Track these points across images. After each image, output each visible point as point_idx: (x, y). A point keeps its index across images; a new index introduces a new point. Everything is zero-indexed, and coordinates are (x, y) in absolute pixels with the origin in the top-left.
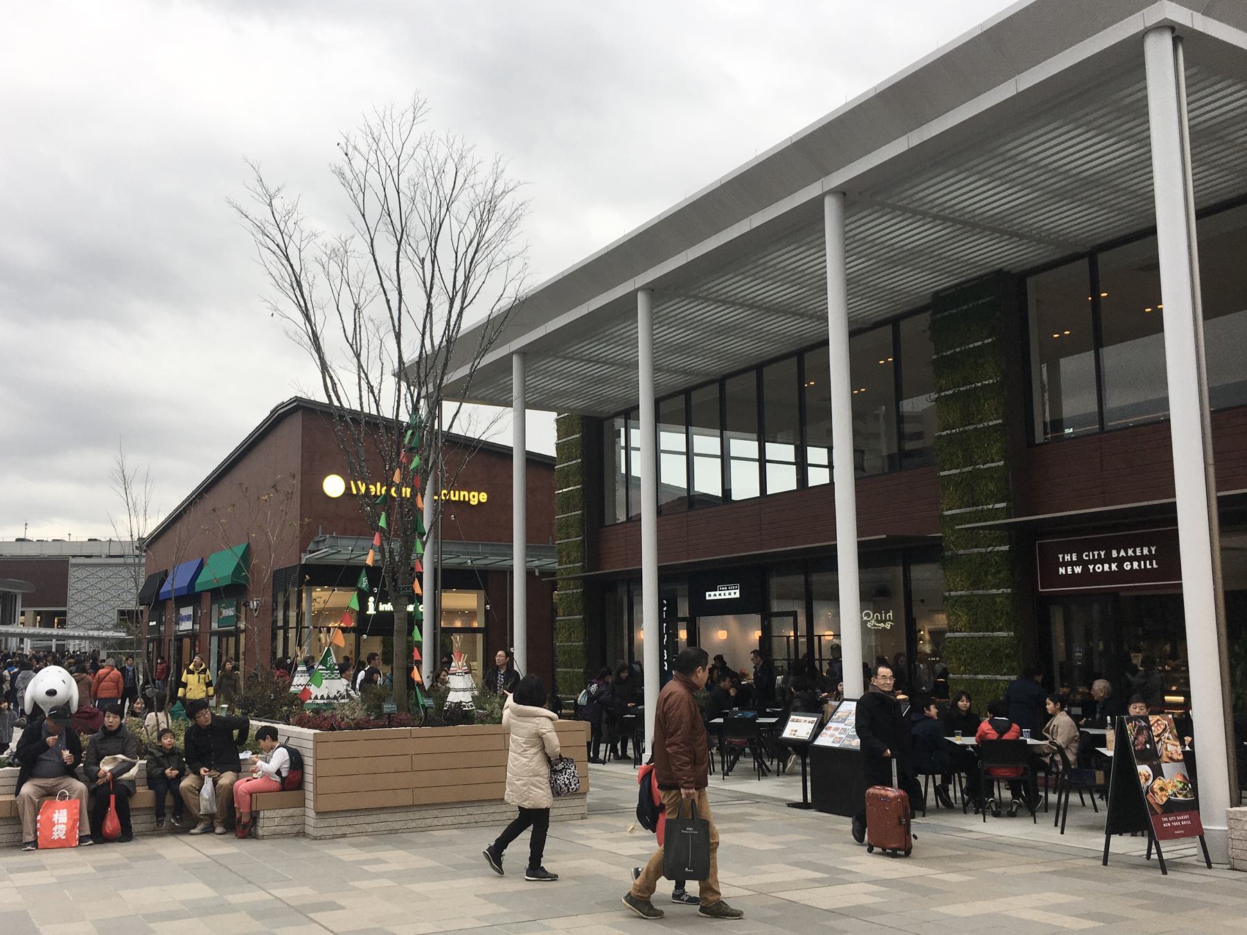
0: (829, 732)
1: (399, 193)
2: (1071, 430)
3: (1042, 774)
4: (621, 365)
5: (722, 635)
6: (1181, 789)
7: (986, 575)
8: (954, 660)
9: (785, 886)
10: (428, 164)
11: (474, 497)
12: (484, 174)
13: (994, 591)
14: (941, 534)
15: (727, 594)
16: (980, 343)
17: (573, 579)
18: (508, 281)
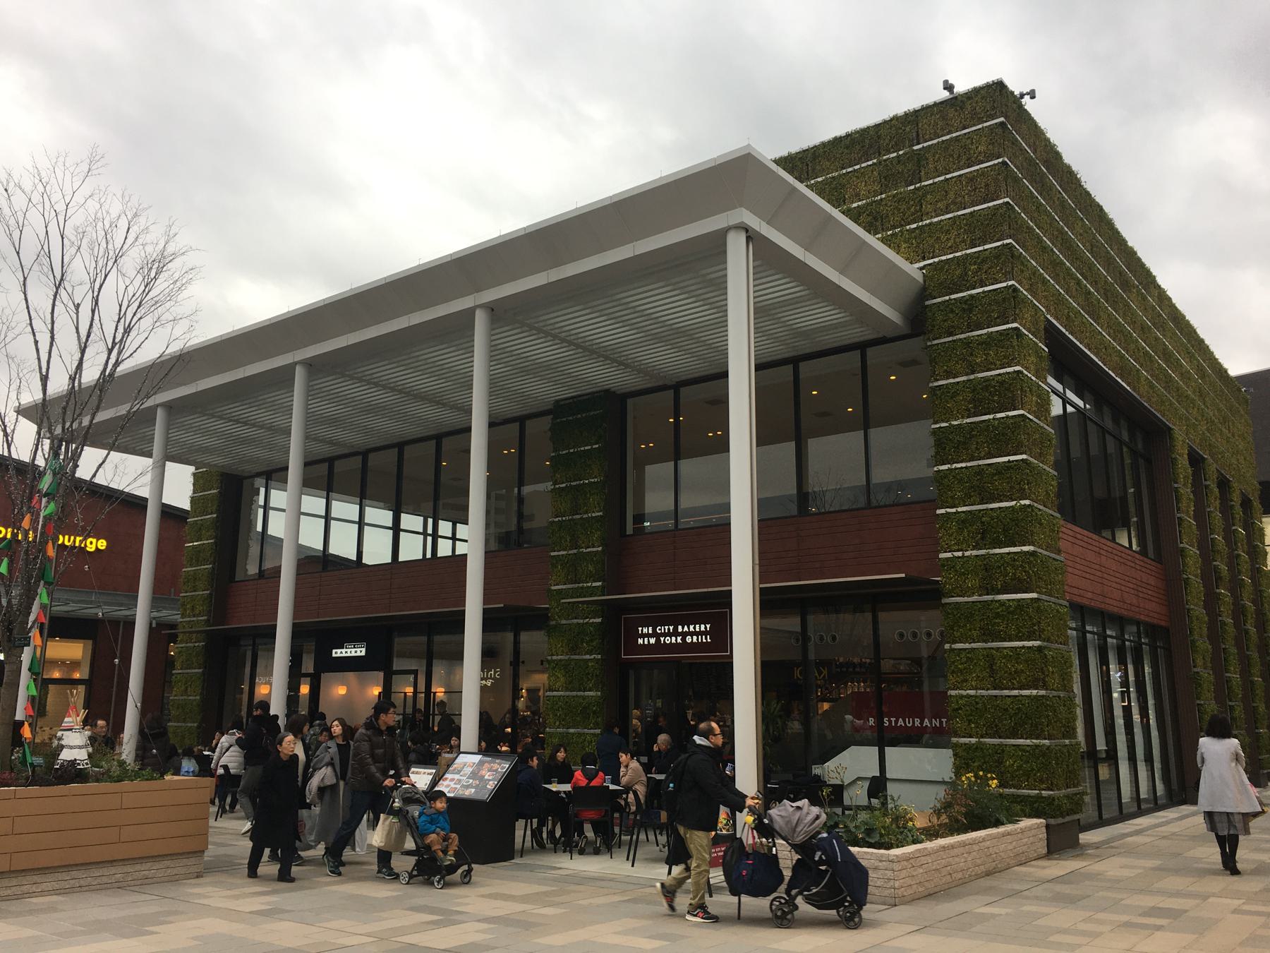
0: (446, 783)
1: (63, 238)
2: (649, 524)
3: (616, 815)
4: (270, 429)
5: (342, 691)
6: (725, 825)
7: (582, 643)
8: (551, 716)
9: (403, 931)
10: (99, 215)
11: (91, 543)
12: (155, 236)
13: (588, 657)
14: (547, 606)
15: (353, 652)
16: (589, 447)
17: (198, 632)
18: (171, 340)
